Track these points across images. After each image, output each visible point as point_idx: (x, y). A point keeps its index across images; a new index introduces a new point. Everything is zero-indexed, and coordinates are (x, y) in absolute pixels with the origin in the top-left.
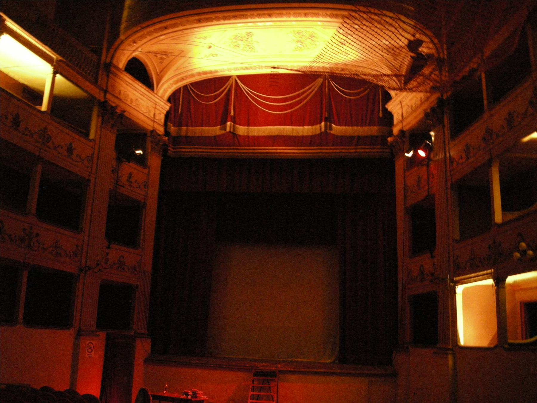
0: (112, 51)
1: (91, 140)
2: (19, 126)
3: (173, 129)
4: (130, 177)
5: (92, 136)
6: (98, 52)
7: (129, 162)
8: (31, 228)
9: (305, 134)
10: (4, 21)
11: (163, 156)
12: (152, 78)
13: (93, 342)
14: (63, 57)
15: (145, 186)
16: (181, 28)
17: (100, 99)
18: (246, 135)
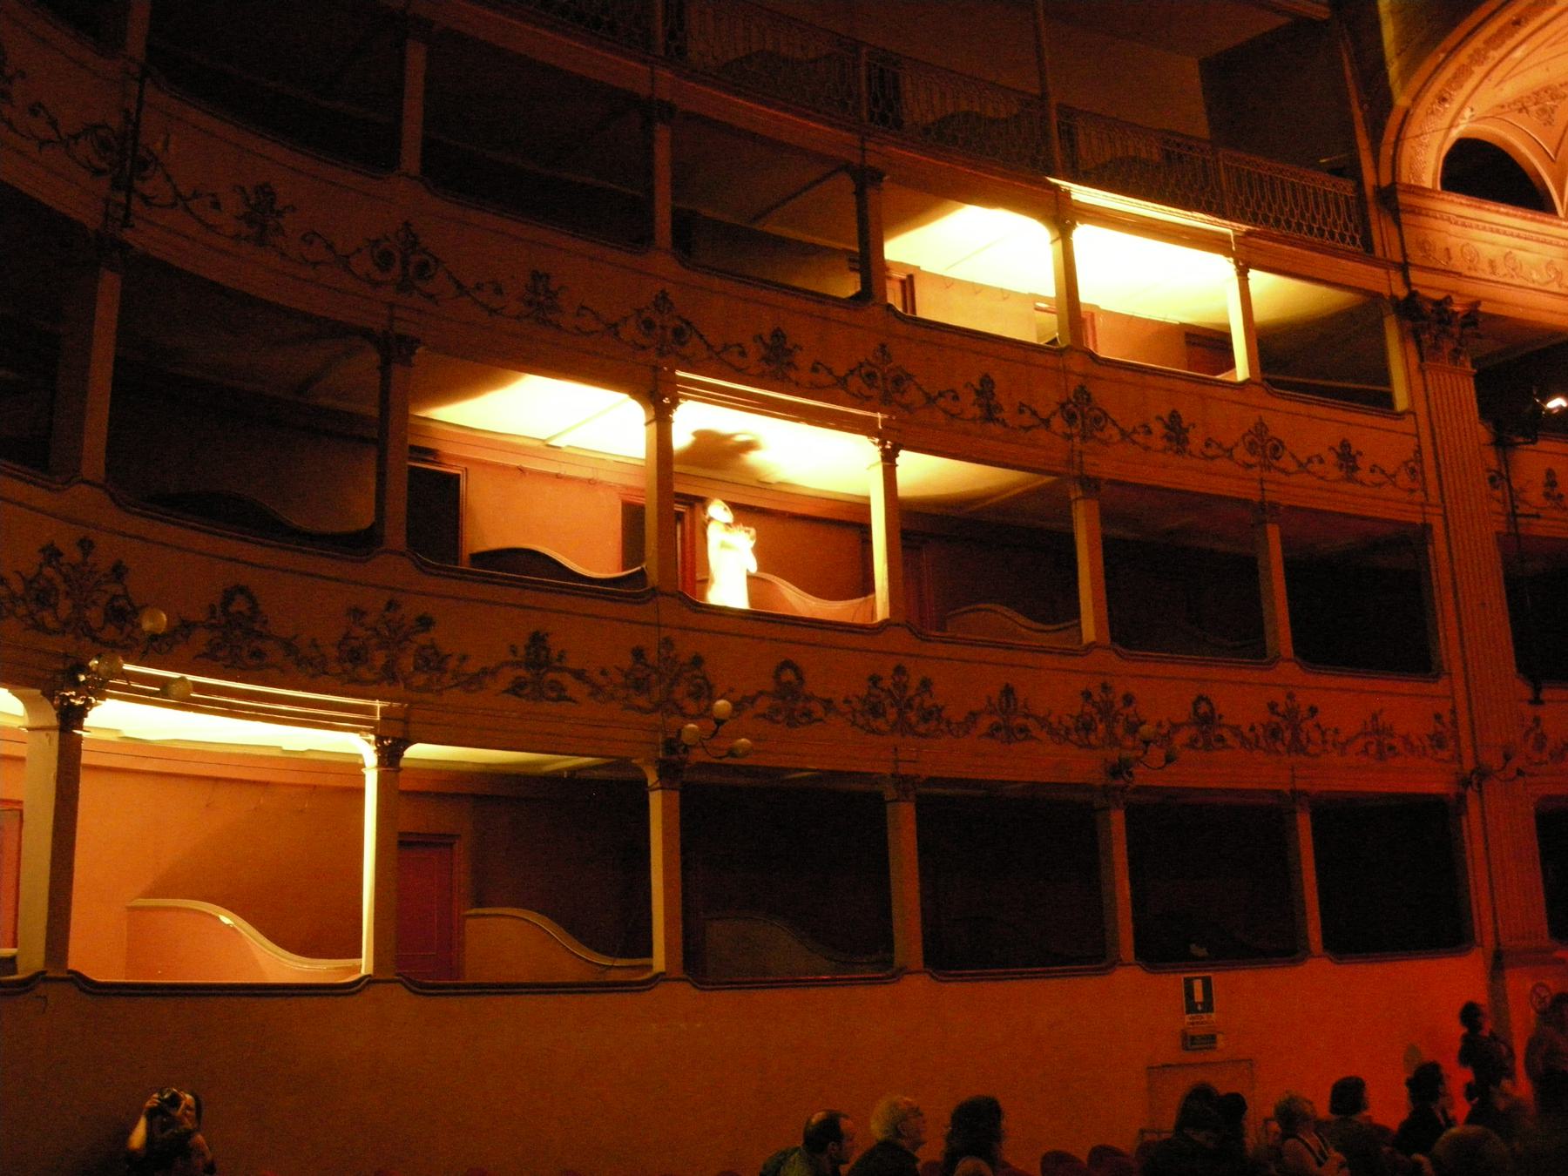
0: (1386, 151)
1: (1401, 415)
4: (1551, 480)
5: (1401, 401)
6: (1350, 170)
7: (1534, 442)
8: (1291, 696)
10: (1068, 193)
12: (1539, 176)
14: (1254, 220)
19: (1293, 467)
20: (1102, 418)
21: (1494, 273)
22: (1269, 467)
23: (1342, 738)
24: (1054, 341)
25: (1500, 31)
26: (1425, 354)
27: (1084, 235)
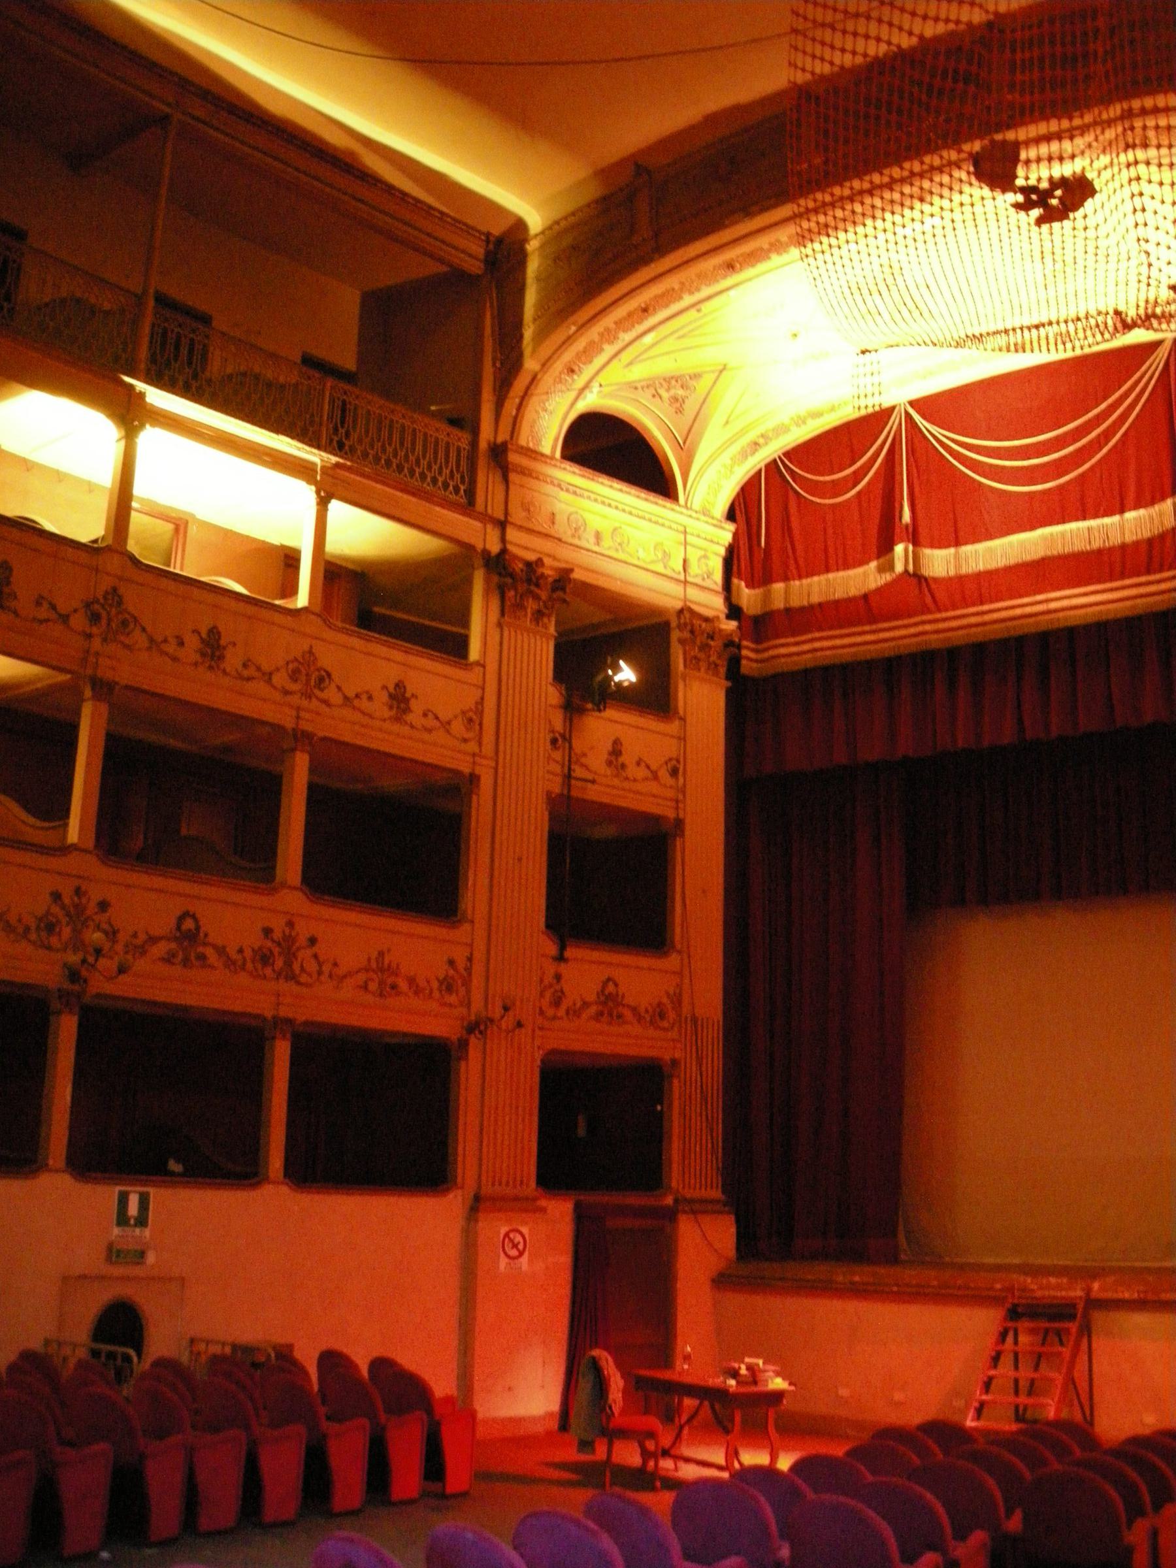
0: (510, 407)
2: (221, 658)
3: (747, 596)
4: (616, 750)
5: (474, 653)
8: (291, 924)
9: (1129, 538)
10: (142, 395)
11: (727, 678)
13: (525, 1230)
15: (674, 772)
16: (688, 300)
17: (488, 547)
18: (952, 573)
19: (337, 699)
20: (128, 623)
21: (598, 544)
22: (309, 697)
23: (341, 971)
24: (96, 541)
25: (630, 315)
26: (509, 609)
27: (150, 438)
